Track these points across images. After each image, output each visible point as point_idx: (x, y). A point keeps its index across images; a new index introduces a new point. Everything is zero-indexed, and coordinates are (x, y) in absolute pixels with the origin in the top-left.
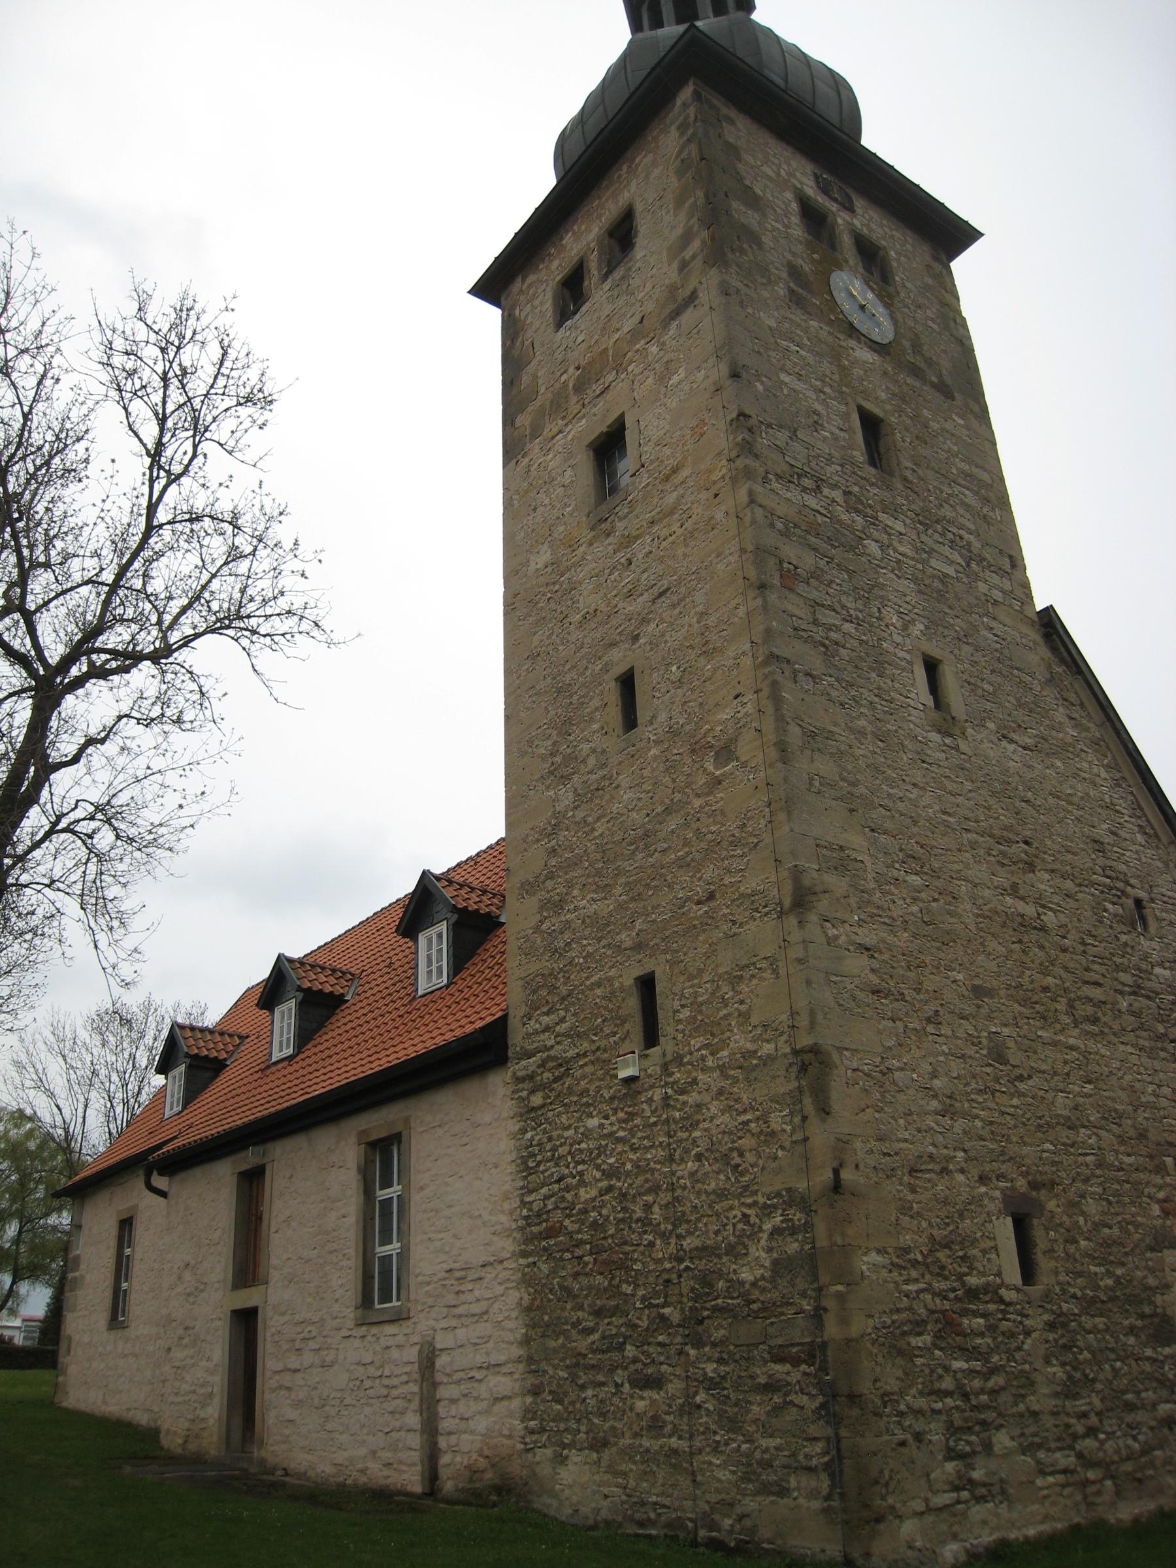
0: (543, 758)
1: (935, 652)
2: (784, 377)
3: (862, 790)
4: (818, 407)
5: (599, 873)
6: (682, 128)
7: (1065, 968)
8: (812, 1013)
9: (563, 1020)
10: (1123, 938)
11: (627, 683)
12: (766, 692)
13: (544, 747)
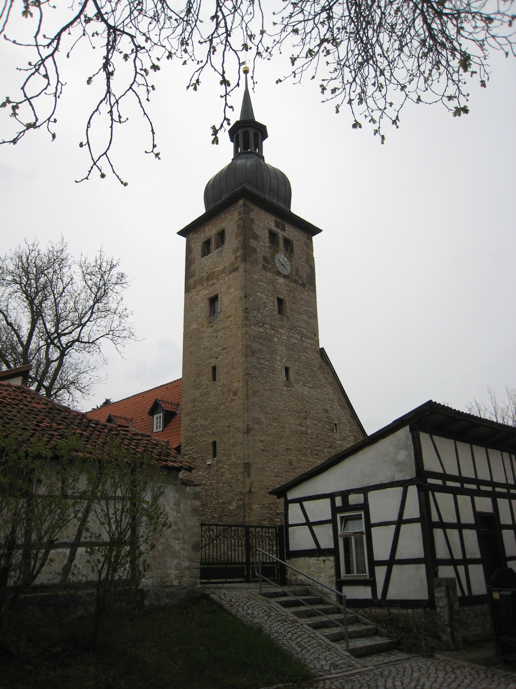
0: (193, 382)
1: (288, 365)
2: (258, 294)
3: (265, 404)
4: (266, 301)
5: (205, 415)
6: (240, 213)
7: (311, 443)
8: (248, 456)
9: (194, 448)
10: (329, 434)
11: (214, 368)
12: (245, 382)
13: (193, 379)
